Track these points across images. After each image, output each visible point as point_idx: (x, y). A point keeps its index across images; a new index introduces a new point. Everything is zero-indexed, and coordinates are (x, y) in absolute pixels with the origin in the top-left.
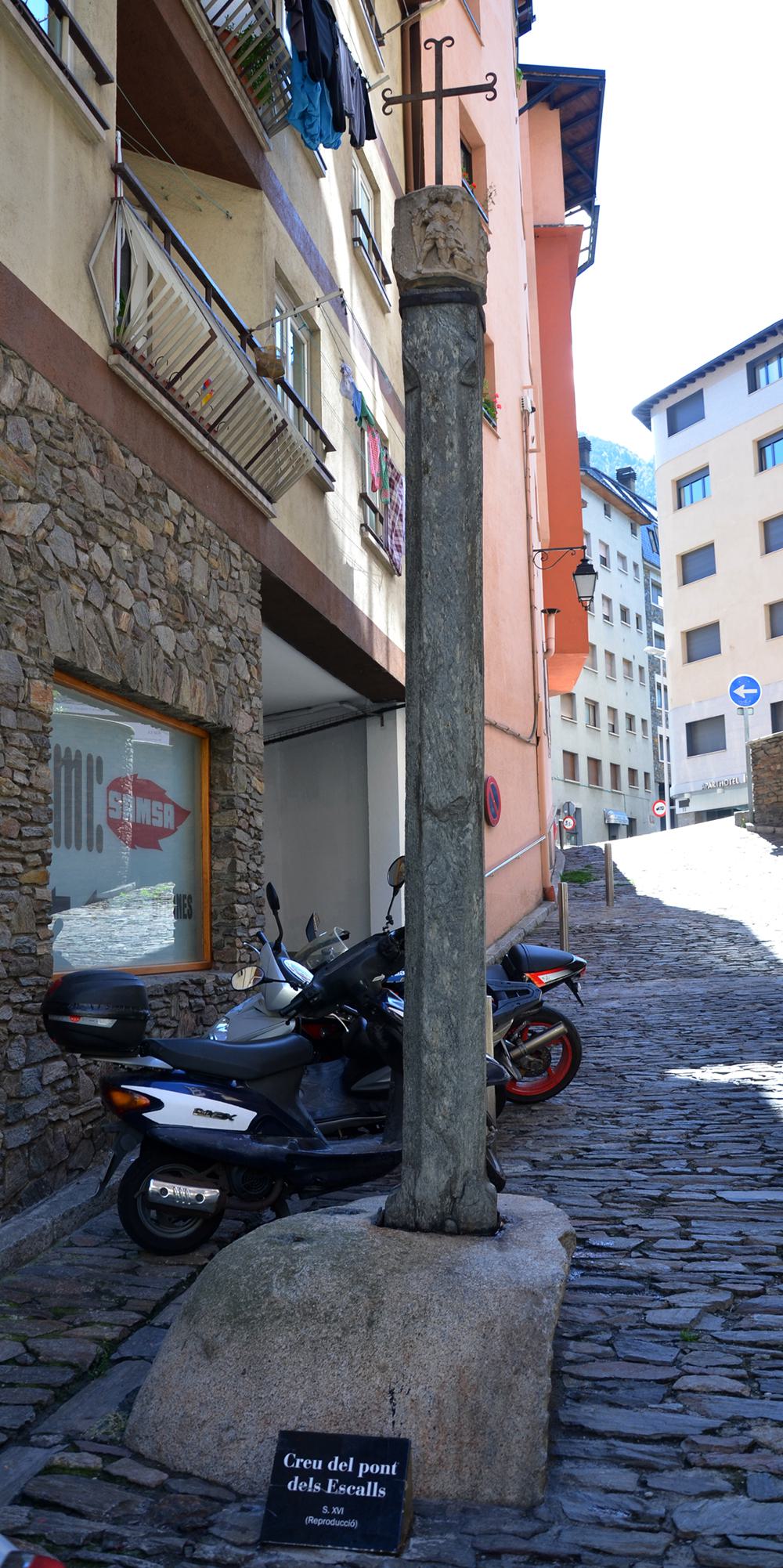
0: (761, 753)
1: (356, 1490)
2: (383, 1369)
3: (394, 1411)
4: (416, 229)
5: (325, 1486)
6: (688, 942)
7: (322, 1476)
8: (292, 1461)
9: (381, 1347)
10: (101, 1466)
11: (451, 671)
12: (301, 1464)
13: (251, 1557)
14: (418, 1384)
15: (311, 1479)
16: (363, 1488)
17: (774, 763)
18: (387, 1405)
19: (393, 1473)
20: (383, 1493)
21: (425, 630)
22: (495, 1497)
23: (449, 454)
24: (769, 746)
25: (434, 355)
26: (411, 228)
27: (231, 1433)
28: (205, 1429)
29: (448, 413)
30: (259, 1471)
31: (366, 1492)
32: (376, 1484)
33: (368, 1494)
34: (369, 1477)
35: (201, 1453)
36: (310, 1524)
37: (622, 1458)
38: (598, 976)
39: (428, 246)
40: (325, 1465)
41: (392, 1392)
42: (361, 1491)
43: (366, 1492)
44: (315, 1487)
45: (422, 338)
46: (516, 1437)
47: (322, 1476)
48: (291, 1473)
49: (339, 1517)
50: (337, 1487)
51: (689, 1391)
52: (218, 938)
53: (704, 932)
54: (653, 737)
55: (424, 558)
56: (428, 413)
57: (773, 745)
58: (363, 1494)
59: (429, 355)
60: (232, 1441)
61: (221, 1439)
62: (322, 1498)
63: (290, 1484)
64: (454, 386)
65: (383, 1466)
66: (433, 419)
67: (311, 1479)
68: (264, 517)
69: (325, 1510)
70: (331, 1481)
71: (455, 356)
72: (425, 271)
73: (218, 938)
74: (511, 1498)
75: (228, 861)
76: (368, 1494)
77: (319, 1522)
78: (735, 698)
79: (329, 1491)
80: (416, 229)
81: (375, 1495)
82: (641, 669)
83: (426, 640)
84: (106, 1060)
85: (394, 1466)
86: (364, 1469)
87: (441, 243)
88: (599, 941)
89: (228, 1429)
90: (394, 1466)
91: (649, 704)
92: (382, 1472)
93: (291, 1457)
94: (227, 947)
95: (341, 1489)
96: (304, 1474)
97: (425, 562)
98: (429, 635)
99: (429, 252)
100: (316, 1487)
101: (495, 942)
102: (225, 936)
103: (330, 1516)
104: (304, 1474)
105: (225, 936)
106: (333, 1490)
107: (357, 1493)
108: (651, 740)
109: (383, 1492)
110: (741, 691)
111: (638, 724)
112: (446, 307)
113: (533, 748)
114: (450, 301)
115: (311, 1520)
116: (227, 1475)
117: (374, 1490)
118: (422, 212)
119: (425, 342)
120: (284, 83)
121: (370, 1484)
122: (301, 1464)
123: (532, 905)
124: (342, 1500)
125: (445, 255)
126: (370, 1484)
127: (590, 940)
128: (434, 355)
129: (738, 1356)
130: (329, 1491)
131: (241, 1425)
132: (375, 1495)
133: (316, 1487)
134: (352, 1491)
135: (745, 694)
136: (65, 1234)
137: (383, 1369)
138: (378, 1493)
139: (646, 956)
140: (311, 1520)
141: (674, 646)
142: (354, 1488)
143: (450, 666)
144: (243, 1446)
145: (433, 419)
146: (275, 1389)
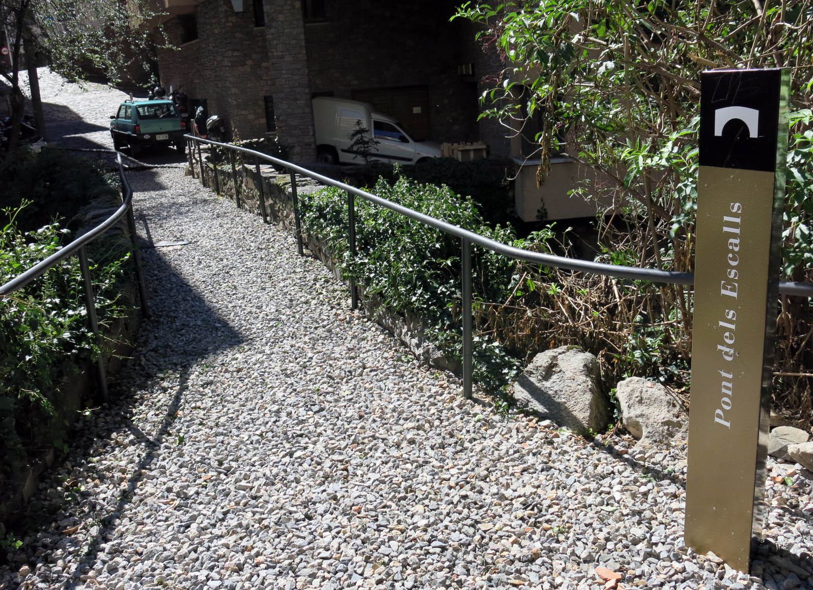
1: (732, 251)
19: (730, 376)
32: (726, 218)
33: (737, 231)
63: (538, 135)
70: (723, 292)
76: (737, 231)
81: (738, 220)
84: (26, 273)
100: (730, 317)
107: (736, 249)
109: (731, 314)
120: (730, 376)
121: (726, 229)
126: (726, 229)
132: (738, 220)
133: (735, 210)
134: (734, 259)
136: (557, 499)
142: (730, 255)
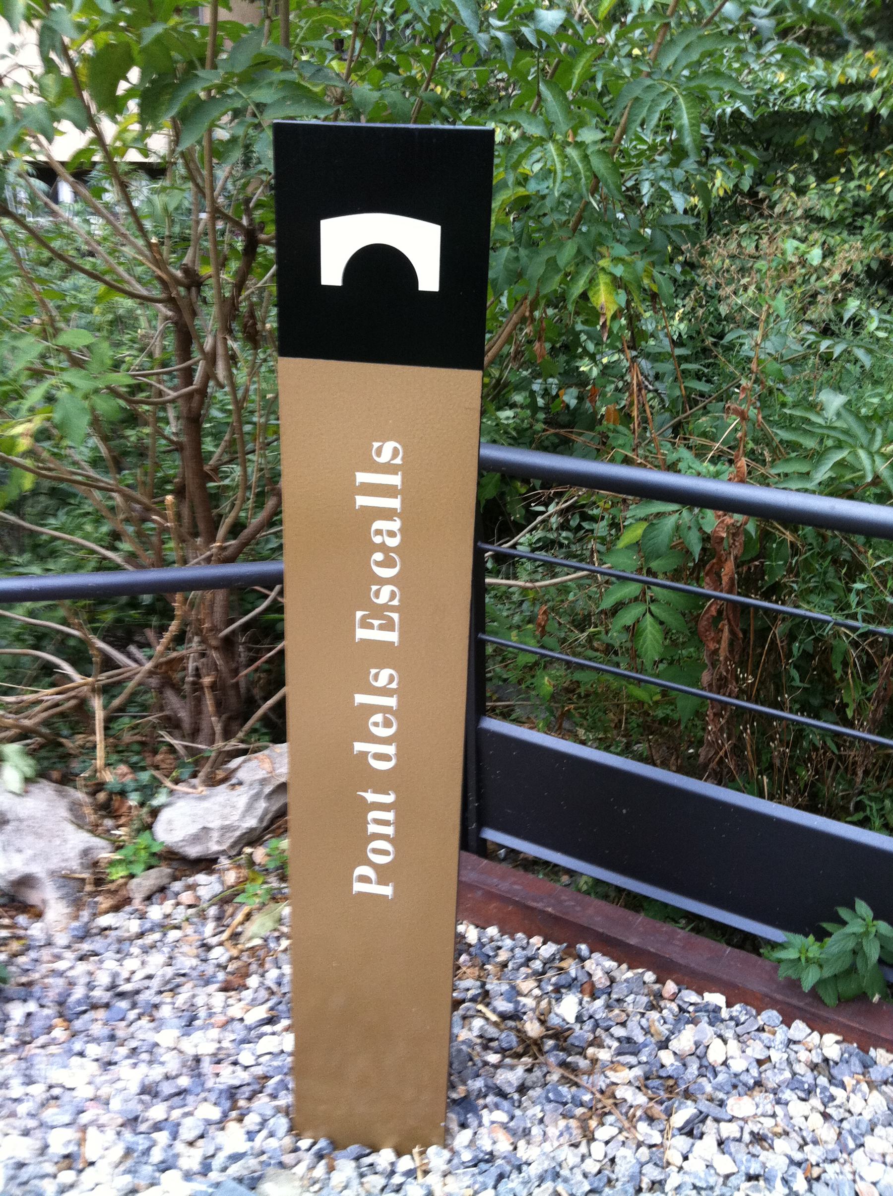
1: (383, 547)
10: (669, 350)
15: (360, 699)
16: (378, 525)
19: (390, 798)
20: (389, 447)
31: (387, 514)
32: (362, 477)
33: (395, 503)
43: (387, 514)
50: (378, 611)
58: (395, 525)
65: (372, 828)
67: (360, 699)
70: (361, 634)
76: (395, 503)
79: (392, 637)
81: (395, 480)
85: (371, 797)
90: (371, 797)
92: (389, 831)
95: (384, 597)
106: (388, 626)
109: (387, 451)
121: (362, 501)
126: (362, 501)
129: (874, 461)
132: (395, 480)
134: (387, 563)
138: (388, 468)
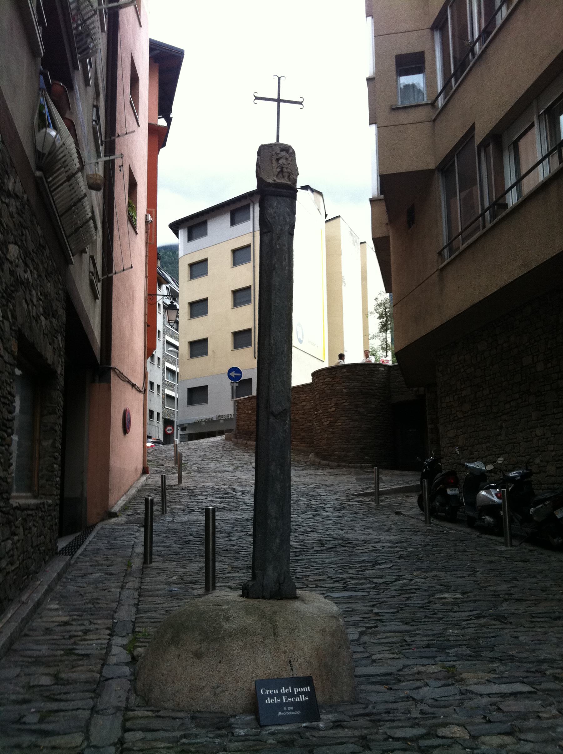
0: (241, 405)
2: (285, 652)
3: (292, 669)
4: (274, 161)
5: (282, 700)
6: (223, 495)
7: (280, 696)
8: (264, 691)
9: (282, 643)
11: (283, 355)
12: (269, 692)
13: (260, 732)
14: (300, 657)
17: (248, 410)
18: (289, 667)
21: (272, 338)
22: (340, 699)
23: (284, 263)
24: (245, 402)
25: (279, 219)
26: (272, 160)
27: (220, 689)
28: (205, 690)
29: (284, 245)
30: (237, 703)
34: (299, 693)
35: (205, 701)
36: (280, 716)
37: (373, 682)
38: (184, 510)
39: (279, 170)
40: (279, 691)
41: (290, 662)
42: (298, 699)
44: (276, 700)
45: (274, 210)
46: (344, 674)
47: (280, 696)
48: (266, 697)
49: (292, 711)
50: (287, 699)
51: (379, 659)
52: (42, 482)
53: (229, 490)
54: (163, 395)
55: (272, 306)
56: (276, 244)
57: (248, 401)
59: (277, 218)
60: (221, 692)
61: (215, 693)
62: (281, 706)
63: (266, 701)
64: (287, 234)
66: (278, 247)
68: (69, 262)
69: (285, 709)
71: (288, 220)
72: (278, 181)
73: (42, 482)
74: (346, 699)
75: (51, 441)
77: (284, 714)
78: (230, 377)
80: (274, 161)
82: (159, 359)
83: (272, 342)
86: (296, 690)
87: (285, 170)
88: (178, 494)
89: (217, 688)
91: (162, 377)
93: (263, 690)
94: (47, 486)
96: (272, 696)
97: (273, 308)
98: (274, 340)
99: (279, 172)
101: (125, 493)
102: (47, 480)
103: (288, 711)
104: (272, 696)
105: (47, 480)
108: (161, 396)
109: (307, 698)
110: (233, 374)
111: (156, 387)
112: (285, 198)
113: (142, 395)
114: (287, 197)
115: (280, 714)
116: (221, 708)
117: (303, 698)
118: (277, 154)
119: (275, 212)
122: (269, 692)
123: (139, 475)
124: (291, 704)
125: (286, 175)
127: (173, 493)
128: (279, 219)
130: (284, 701)
131: (224, 685)
135: (235, 376)
137: (285, 652)
139: (204, 501)
140: (280, 714)
141: (185, 349)
143: (282, 354)
144: (227, 694)
145: (278, 247)
146: (238, 667)
